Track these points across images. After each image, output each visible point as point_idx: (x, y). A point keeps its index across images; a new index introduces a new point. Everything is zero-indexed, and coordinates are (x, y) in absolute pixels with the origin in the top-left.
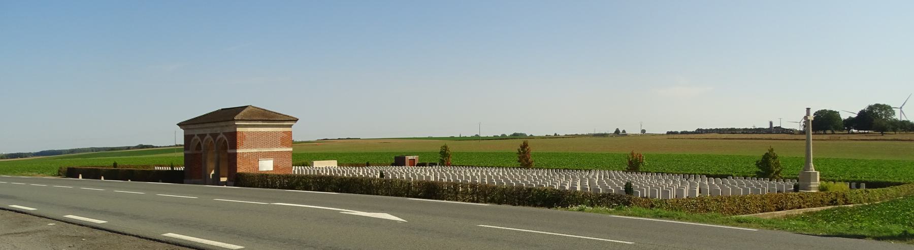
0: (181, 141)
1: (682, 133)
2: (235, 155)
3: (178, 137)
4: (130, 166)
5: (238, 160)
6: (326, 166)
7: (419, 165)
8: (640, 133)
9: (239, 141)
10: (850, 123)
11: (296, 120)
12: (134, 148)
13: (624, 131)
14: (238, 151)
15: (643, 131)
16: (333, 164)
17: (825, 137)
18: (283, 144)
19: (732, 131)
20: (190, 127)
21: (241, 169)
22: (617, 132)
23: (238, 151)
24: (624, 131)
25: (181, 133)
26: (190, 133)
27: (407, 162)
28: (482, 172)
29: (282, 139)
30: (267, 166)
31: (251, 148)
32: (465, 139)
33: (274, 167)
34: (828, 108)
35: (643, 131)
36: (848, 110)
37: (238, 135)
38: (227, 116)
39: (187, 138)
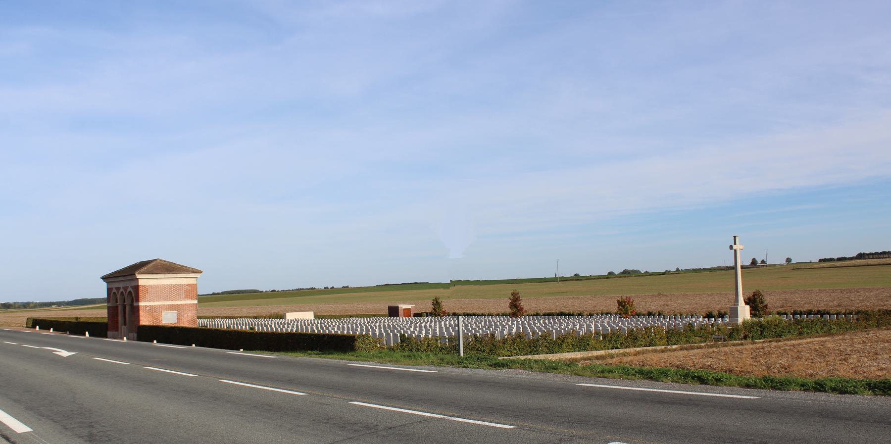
0: (104, 295)
2: (138, 307)
3: (101, 291)
4: (97, 318)
5: (141, 312)
6: (299, 318)
7: (416, 315)
8: (784, 262)
9: (141, 294)
11: (200, 272)
12: (59, 304)
13: (763, 262)
14: (141, 304)
15: (789, 260)
16: (309, 316)
18: (187, 297)
19: (387, 286)
20: (110, 280)
21: (144, 321)
23: (141, 304)
24: (763, 262)
25: (104, 285)
26: (111, 286)
27: (401, 313)
28: (597, 322)
29: (186, 291)
30: (169, 319)
31: (154, 301)
32: (218, 294)
33: (178, 319)
35: (789, 260)
37: (141, 289)
38: (130, 272)
39: (109, 290)
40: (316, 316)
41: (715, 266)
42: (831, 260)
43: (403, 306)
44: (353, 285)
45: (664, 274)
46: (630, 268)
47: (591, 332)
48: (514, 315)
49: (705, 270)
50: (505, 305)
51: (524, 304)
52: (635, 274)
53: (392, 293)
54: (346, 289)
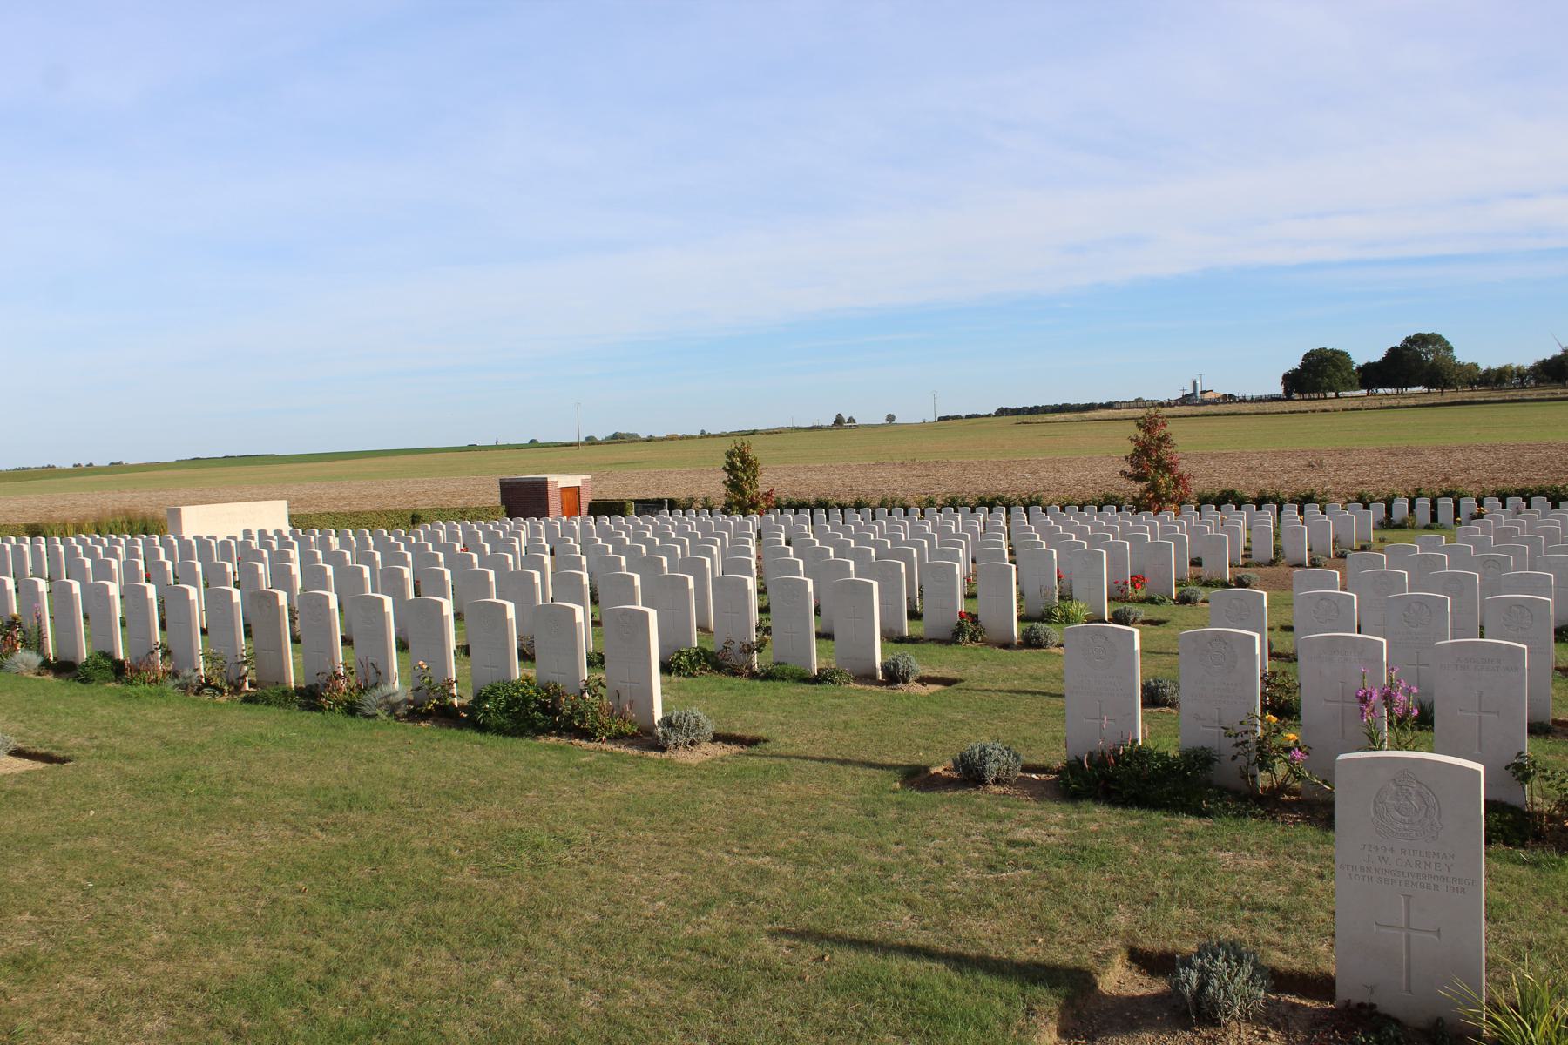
1: (968, 417)
10: (1372, 376)
13: (851, 420)
15: (891, 418)
17: (1327, 405)
19: (196, 462)
22: (839, 421)
24: (851, 420)
34: (1338, 348)
35: (891, 418)
36: (1367, 351)
40: (294, 520)
41: (773, 427)
42: (49, 472)
43: (559, 481)
44: (1238, 393)
45: (721, 436)
46: (624, 431)
47: (1183, 996)
48: (1151, 502)
49: (229, 460)
50: (715, 485)
51: (764, 482)
52: (632, 439)
53: (206, 471)
54: (116, 467)
